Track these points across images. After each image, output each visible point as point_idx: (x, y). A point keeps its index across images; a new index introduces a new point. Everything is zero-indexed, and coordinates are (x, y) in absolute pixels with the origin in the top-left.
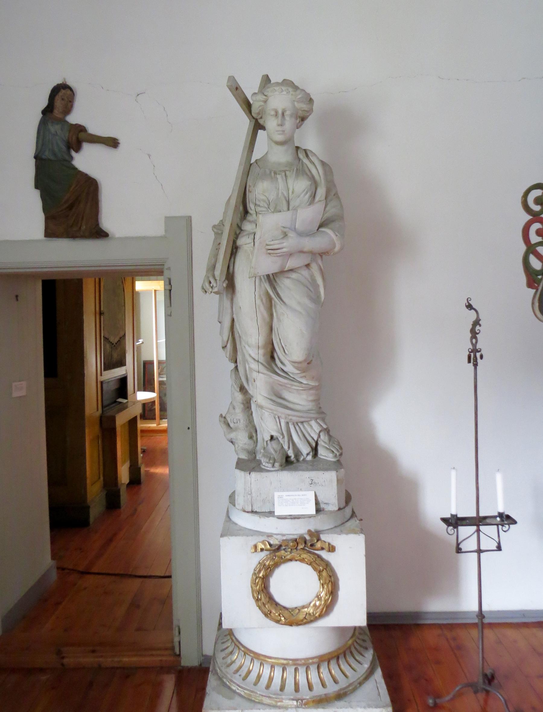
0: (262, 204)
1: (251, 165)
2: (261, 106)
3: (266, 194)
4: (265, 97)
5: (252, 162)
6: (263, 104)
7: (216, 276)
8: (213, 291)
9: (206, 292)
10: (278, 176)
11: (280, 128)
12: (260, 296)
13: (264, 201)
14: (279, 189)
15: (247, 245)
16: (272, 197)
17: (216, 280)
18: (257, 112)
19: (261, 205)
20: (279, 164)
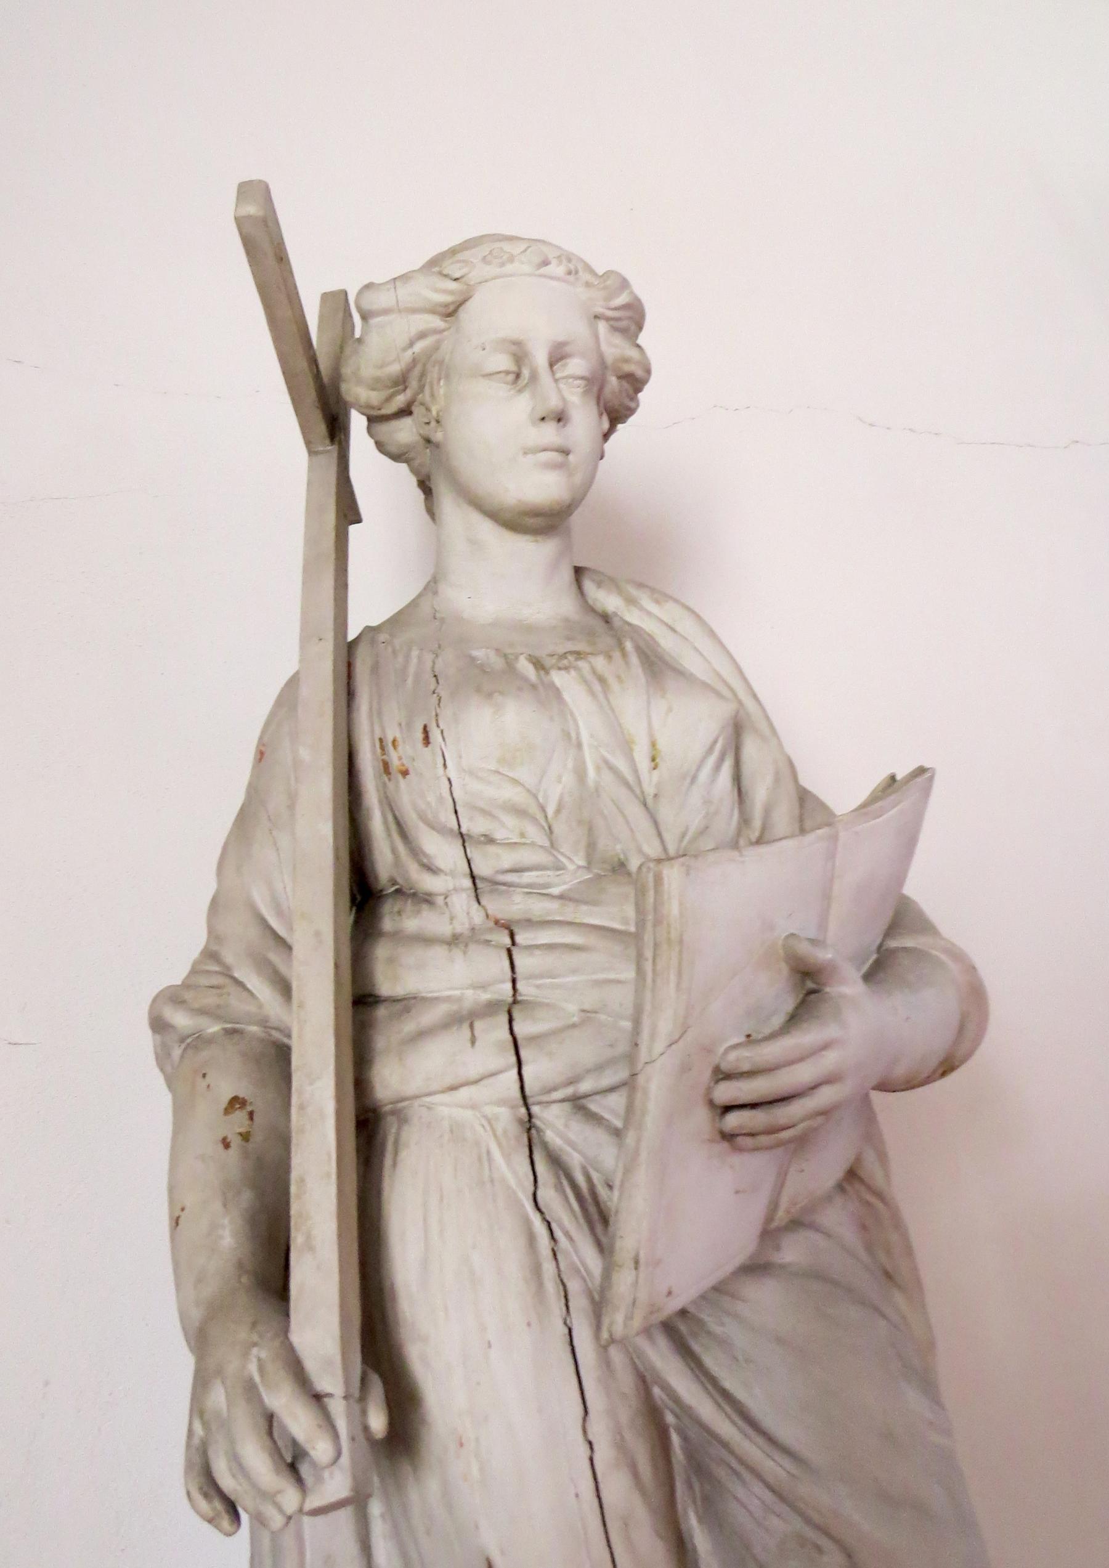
0: (507, 828)
1: (352, 646)
2: (422, 335)
3: (524, 774)
4: (454, 286)
5: (351, 637)
6: (437, 322)
7: (311, 1366)
8: (314, 1501)
9: (232, 1509)
10: (558, 678)
11: (549, 433)
12: (620, 1446)
13: (520, 812)
14: (579, 746)
15: (464, 1094)
16: (556, 788)
17: (318, 1398)
18: (395, 369)
19: (499, 835)
20: (528, 629)
